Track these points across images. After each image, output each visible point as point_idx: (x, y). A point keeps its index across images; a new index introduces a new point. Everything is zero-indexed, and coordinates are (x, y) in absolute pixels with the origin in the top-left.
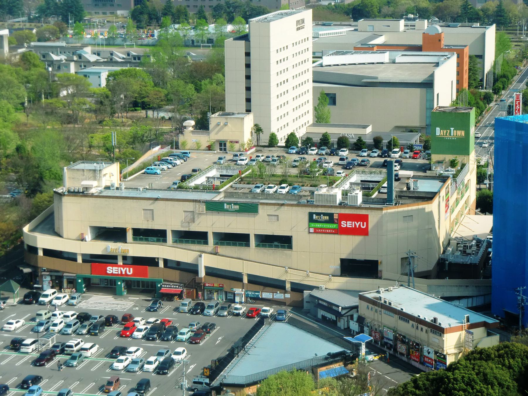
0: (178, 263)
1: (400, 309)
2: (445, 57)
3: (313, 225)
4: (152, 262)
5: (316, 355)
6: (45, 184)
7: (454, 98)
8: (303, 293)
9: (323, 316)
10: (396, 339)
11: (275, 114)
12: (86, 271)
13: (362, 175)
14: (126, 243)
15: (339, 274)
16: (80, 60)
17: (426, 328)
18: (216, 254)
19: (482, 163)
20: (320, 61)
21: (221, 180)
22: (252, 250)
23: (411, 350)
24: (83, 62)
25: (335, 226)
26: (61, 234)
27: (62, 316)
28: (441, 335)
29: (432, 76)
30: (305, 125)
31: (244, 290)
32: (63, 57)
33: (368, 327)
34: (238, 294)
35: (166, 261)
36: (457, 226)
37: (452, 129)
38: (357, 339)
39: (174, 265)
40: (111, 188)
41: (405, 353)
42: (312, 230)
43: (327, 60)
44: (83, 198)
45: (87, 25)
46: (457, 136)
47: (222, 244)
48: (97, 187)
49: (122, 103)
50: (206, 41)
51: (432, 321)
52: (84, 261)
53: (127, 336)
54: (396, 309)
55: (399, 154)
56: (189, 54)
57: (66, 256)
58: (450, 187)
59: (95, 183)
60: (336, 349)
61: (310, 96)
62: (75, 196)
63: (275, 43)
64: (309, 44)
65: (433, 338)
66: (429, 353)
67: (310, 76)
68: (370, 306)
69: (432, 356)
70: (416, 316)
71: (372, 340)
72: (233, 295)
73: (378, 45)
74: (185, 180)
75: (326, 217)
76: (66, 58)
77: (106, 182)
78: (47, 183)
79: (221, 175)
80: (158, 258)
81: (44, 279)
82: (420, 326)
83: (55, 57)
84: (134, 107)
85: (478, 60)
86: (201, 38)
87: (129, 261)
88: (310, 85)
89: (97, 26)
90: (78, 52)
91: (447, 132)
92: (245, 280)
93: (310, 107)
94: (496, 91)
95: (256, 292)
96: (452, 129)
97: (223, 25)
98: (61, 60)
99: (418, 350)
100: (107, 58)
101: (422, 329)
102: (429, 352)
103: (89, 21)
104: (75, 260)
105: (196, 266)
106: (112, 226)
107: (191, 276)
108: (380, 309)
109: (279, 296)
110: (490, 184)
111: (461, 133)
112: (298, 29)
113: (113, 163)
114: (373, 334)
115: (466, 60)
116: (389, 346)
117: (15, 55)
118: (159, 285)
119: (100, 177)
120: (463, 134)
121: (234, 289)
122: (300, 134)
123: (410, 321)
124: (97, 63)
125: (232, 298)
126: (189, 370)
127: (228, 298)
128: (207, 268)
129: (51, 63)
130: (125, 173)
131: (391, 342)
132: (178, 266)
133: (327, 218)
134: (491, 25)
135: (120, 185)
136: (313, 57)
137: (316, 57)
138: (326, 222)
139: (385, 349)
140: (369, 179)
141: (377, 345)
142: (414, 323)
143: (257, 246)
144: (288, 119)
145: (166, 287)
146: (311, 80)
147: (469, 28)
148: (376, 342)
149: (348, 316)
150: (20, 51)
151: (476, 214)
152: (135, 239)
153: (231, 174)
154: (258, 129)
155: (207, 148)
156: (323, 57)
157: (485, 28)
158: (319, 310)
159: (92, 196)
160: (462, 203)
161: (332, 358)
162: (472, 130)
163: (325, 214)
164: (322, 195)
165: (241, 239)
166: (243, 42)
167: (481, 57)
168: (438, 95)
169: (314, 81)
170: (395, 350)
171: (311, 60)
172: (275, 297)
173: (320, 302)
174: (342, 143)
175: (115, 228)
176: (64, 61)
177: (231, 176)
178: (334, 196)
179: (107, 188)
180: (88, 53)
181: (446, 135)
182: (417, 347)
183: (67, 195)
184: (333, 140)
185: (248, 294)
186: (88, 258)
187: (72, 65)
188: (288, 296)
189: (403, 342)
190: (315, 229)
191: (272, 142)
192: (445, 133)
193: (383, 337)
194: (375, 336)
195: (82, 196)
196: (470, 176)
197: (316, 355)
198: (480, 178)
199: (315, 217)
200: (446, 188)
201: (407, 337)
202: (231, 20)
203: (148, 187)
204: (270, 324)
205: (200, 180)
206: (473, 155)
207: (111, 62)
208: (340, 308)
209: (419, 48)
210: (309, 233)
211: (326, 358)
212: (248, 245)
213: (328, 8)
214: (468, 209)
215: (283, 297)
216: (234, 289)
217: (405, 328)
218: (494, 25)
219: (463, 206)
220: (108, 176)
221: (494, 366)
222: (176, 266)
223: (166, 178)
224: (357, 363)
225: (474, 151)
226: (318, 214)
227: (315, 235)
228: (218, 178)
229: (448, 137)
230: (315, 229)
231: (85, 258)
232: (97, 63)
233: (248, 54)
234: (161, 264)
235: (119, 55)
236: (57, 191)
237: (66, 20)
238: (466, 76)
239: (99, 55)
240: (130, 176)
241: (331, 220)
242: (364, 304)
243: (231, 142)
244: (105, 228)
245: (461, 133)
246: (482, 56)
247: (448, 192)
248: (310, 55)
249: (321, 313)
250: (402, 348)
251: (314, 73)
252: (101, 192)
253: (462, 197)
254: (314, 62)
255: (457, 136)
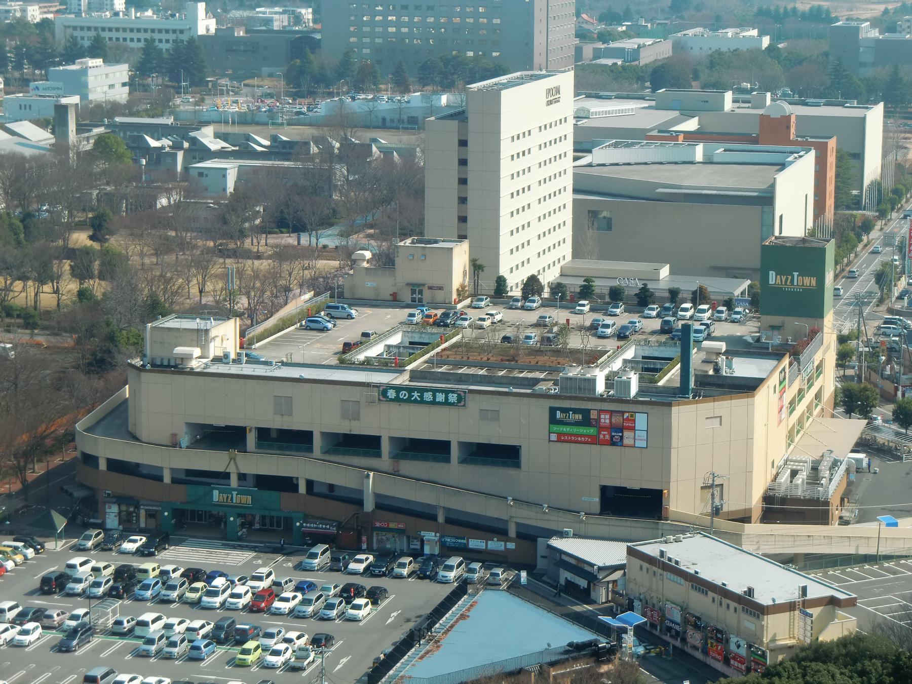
0: (331, 487)
1: (692, 572)
2: (796, 155)
3: (555, 428)
4: (286, 484)
5: (549, 645)
6: (119, 352)
7: (810, 225)
8: (536, 541)
9: (568, 582)
10: (686, 621)
11: (506, 243)
12: (181, 496)
13: (645, 348)
14: (245, 452)
15: (598, 510)
16: (194, 147)
17: (736, 605)
18: (396, 473)
19: (845, 332)
20: (587, 159)
21: (411, 351)
22: (454, 470)
23: (709, 641)
24: (200, 152)
25: (592, 431)
26: (138, 436)
27: (157, 572)
28: (758, 617)
29: (772, 187)
30: (559, 262)
31: (438, 535)
32: (166, 142)
33: (641, 600)
34: (429, 541)
35: (310, 484)
36: (800, 435)
37: (796, 274)
38: (621, 620)
39: (325, 491)
40: (224, 360)
41: (699, 645)
42: (554, 437)
43: (599, 155)
44: (176, 377)
45: (210, 90)
46: (803, 285)
47: (405, 458)
48: (200, 357)
49: (258, 222)
50: (406, 121)
51: (745, 592)
52: (174, 481)
53: (260, 611)
54: (687, 572)
55: (708, 314)
56: (375, 140)
57: (145, 471)
58: (787, 370)
59: (197, 352)
60: (582, 635)
61: (567, 215)
62: (163, 372)
63: (509, 124)
64: (568, 129)
65: (748, 623)
66: (739, 646)
67: (568, 181)
68: (646, 565)
69: (743, 651)
70: (720, 584)
71: (645, 623)
72: (419, 543)
73: (685, 133)
74: (350, 350)
75: (577, 416)
76: (171, 143)
77: (215, 350)
78: (124, 350)
79: (411, 343)
80: (297, 478)
81: (108, 510)
82: (725, 601)
83: (153, 143)
84: (278, 227)
85: (852, 162)
86: (397, 116)
87: (250, 481)
88: (568, 198)
89: (228, 93)
90: (192, 134)
91: (787, 279)
92: (441, 519)
93: (567, 232)
94: (882, 214)
95: (458, 538)
96: (796, 274)
97: (435, 92)
98: (163, 148)
99: (719, 640)
100: (239, 146)
101: (728, 606)
102: (737, 646)
103: (215, 84)
104: (160, 479)
105: (361, 492)
106: (222, 424)
107: (351, 509)
108: (660, 571)
109: (496, 545)
110: (860, 368)
111: (810, 282)
112: (550, 103)
113: (229, 319)
114: (649, 614)
115: (831, 159)
116: (673, 632)
117: (88, 139)
118: (298, 524)
119: (206, 340)
120: (814, 282)
121: (423, 533)
122: (548, 278)
123: (709, 593)
124: (222, 154)
125: (418, 547)
126: (339, 667)
127: (412, 547)
128: (377, 496)
129: (147, 150)
130: (251, 335)
131: (677, 627)
132: (331, 492)
133: (579, 417)
134: (876, 103)
135: (239, 355)
136: (575, 151)
137: (582, 147)
138: (577, 424)
139: (667, 638)
140: (656, 354)
141: (654, 632)
142: (716, 596)
143: (463, 461)
144: (529, 253)
145: (310, 527)
146: (570, 189)
147: (840, 108)
148: (653, 626)
149: (608, 582)
150: (97, 131)
151: (833, 416)
152: (259, 446)
153: (427, 341)
154: (476, 267)
155: (391, 298)
156: (594, 150)
157: (867, 108)
158: (561, 570)
159: (192, 373)
160: (810, 396)
161: (576, 650)
162: (829, 276)
163: (575, 411)
164: (571, 379)
165: (436, 450)
166: (454, 124)
167: (859, 156)
168: (781, 217)
169: (576, 191)
170: (684, 640)
171: (571, 154)
172: (489, 547)
173: (564, 557)
174: (616, 295)
175: (227, 427)
176: (167, 149)
177: (427, 344)
178: (593, 381)
179: (217, 360)
180: (207, 137)
181: (786, 284)
182: (719, 636)
183: (149, 371)
184: (601, 286)
185: (445, 542)
186: (182, 476)
187: (180, 156)
188: (511, 546)
189: (697, 627)
190: (560, 435)
191: (500, 290)
192: (784, 280)
193: (663, 617)
194: (652, 616)
195: (173, 373)
196: (826, 352)
197: (549, 645)
198: (843, 358)
199: (559, 415)
200: (781, 372)
201: (703, 618)
202: (447, 87)
203: (285, 360)
204: (477, 592)
205: (375, 351)
206: (829, 319)
207: (245, 152)
208: (596, 567)
209: (755, 141)
210: (550, 441)
211: (566, 652)
212: (447, 460)
213: (612, 71)
214: (819, 408)
215: (502, 548)
216: (423, 533)
217: (701, 603)
218: (882, 104)
219: (811, 402)
220: (218, 340)
221: (837, 672)
222: (327, 492)
223: (318, 345)
224: (617, 661)
225: (832, 312)
226: (565, 410)
227: (559, 444)
228: (404, 347)
229: (788, 288)
230: (560, 435)
231: (175, 476)
232: (222, 154)
233: (463, 143)
234: (302, 489)
235: (262, 142)
236: (133, 363)
237: (176, 78)
238: (830, 188)
239: (225, 140)
240: (259, 340)
241: (586, 421)
242: (637, 562)
243: (430, 288)
244: (211, 426)
245: (810, 282)
246: (859, 154)
247: (784, 379)
248: (568, 146)
249: (565, 575)
250: (695, 638)
251: (576, 177)
252: (207, 366)
253: (809, 388)
254: (576, 159)
255: (803, 285)
